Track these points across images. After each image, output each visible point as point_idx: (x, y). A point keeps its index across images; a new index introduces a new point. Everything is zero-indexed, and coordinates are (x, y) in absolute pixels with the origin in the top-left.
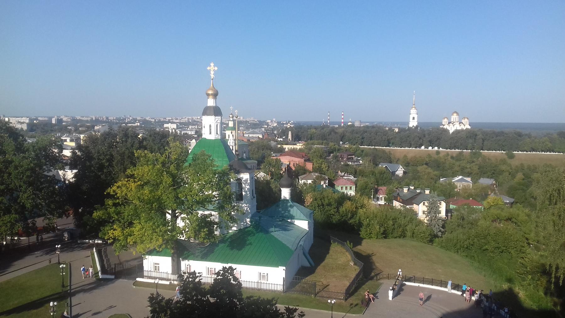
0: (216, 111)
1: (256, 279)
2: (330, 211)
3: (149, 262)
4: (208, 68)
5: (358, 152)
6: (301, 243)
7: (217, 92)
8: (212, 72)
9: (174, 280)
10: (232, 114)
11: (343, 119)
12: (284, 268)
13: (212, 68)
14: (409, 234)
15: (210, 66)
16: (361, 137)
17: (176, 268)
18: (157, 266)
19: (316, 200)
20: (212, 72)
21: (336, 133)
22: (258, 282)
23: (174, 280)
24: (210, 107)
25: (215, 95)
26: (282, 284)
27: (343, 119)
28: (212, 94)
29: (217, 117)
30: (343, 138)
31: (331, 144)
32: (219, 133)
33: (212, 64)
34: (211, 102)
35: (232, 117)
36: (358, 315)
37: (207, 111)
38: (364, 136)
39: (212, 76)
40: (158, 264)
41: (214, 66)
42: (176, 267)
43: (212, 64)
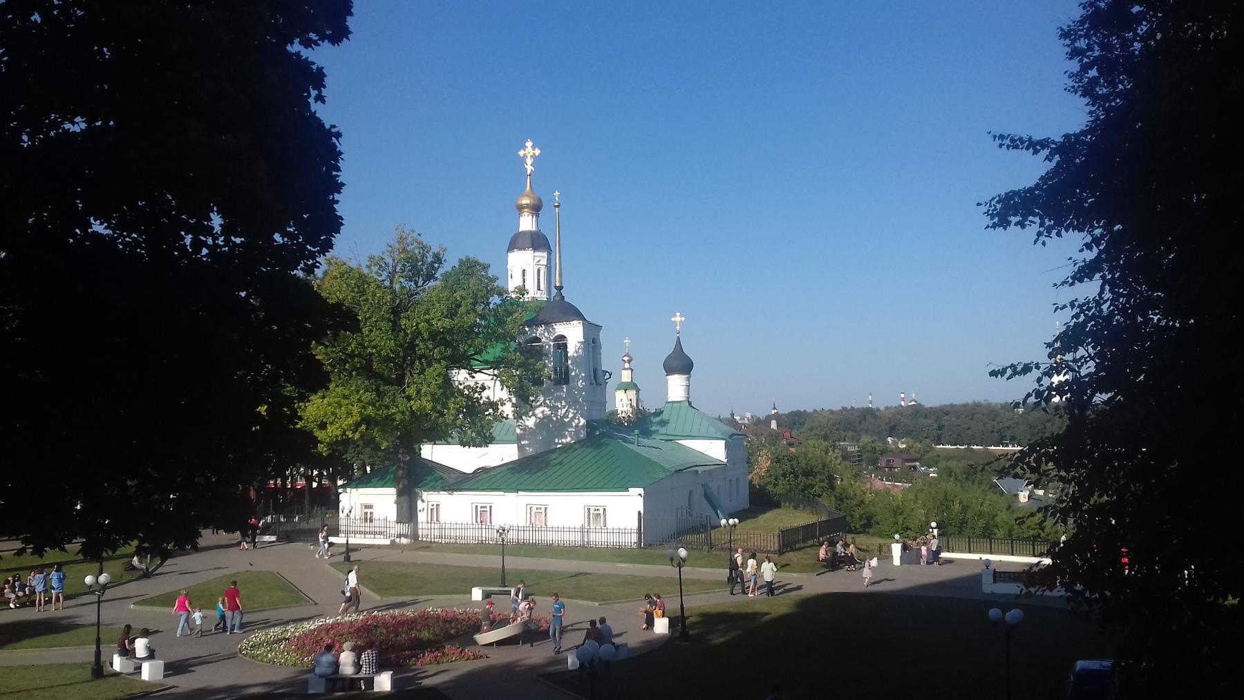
0: (537, 241)
1: (578, 520)
2: (813, 486)
3: (352, 500)
4: (521, 153)
5: (928, 455)
6: (700, 469)
7: (540, 200)
8: (529, 161)
9: (400, 536)
10: (627, 355)
11: (903, 399)
12: (641, 491)
13: (529, 151)
14: (1000, 533)
15: (524, 147)
16: (936, 426)
17: (408, 513)
18: (369, 511)
19: (779, 461)
20: (529, 161)
21: (876, 417)
22: (582, 529)
23: (400, 536)
24: (524, 233)
25: (536, 209)
26: (635, 526)
27: (903, 399)
28: (528, 206)
29: (537, 254)
30: (892, 431)
31: (865, 439)
32: (542, 287)
33: (529, 144)
34: (527, 223)
35: (629, 361)
36: (805, 575)
37: (518, 242)
38: (943, 422)
39: (529, 168)
40: (371, 507)
41: (533, 147)
42: (405, 505)
43: (529, 144)
